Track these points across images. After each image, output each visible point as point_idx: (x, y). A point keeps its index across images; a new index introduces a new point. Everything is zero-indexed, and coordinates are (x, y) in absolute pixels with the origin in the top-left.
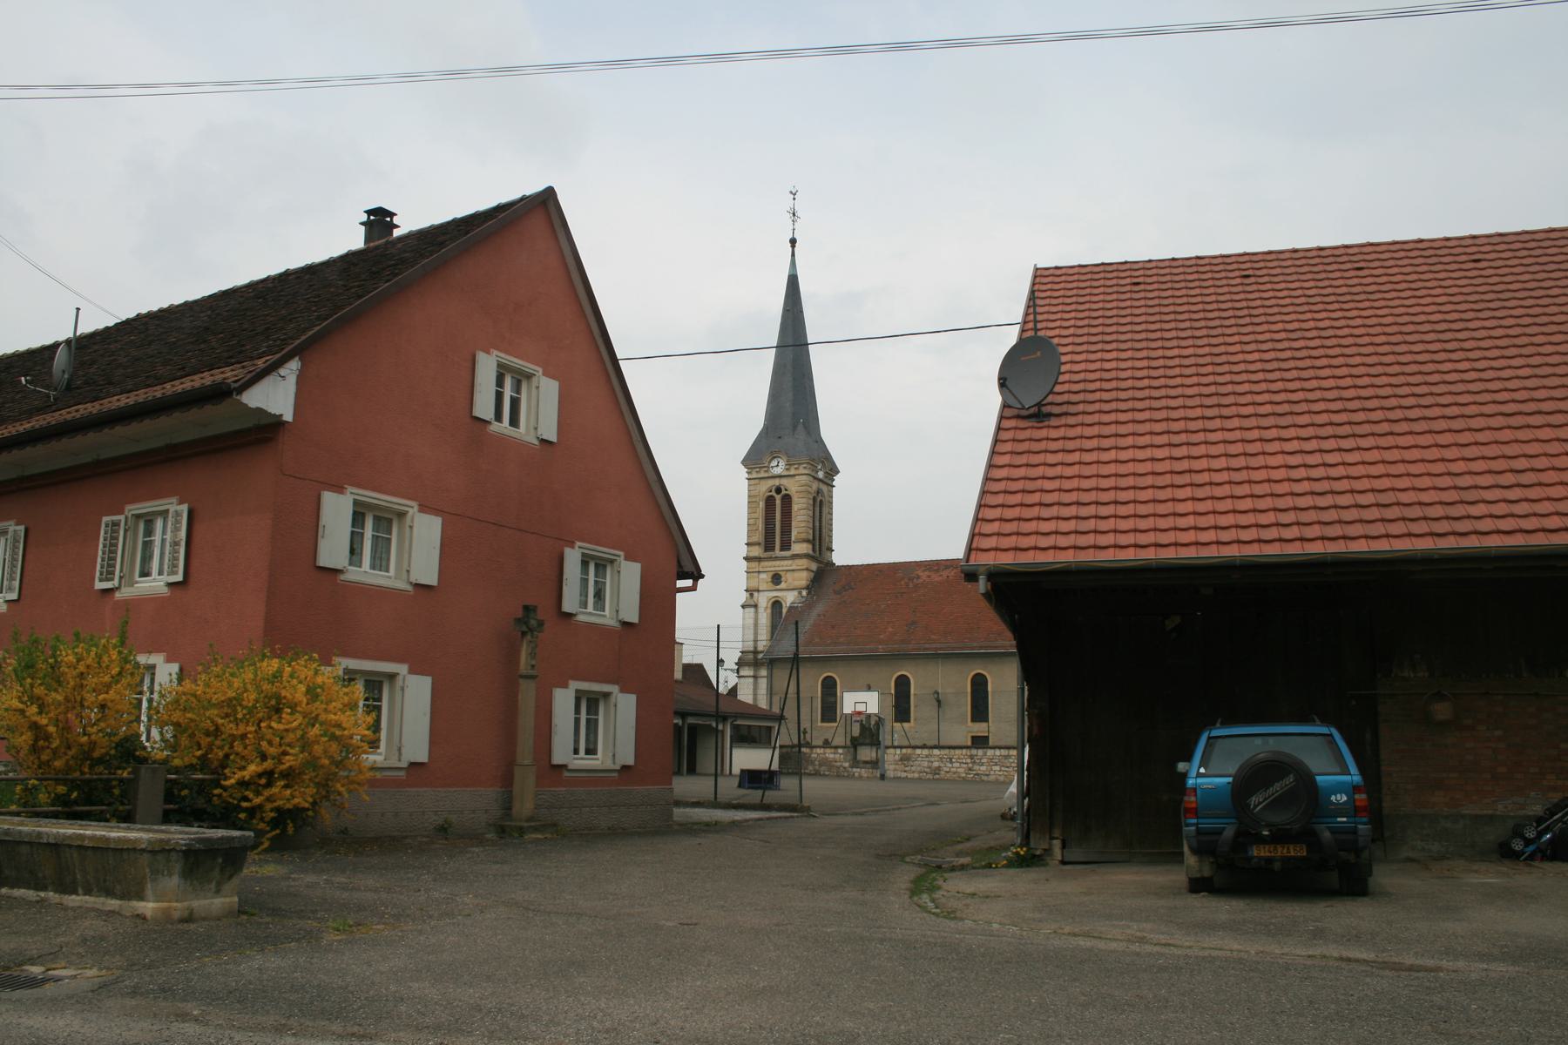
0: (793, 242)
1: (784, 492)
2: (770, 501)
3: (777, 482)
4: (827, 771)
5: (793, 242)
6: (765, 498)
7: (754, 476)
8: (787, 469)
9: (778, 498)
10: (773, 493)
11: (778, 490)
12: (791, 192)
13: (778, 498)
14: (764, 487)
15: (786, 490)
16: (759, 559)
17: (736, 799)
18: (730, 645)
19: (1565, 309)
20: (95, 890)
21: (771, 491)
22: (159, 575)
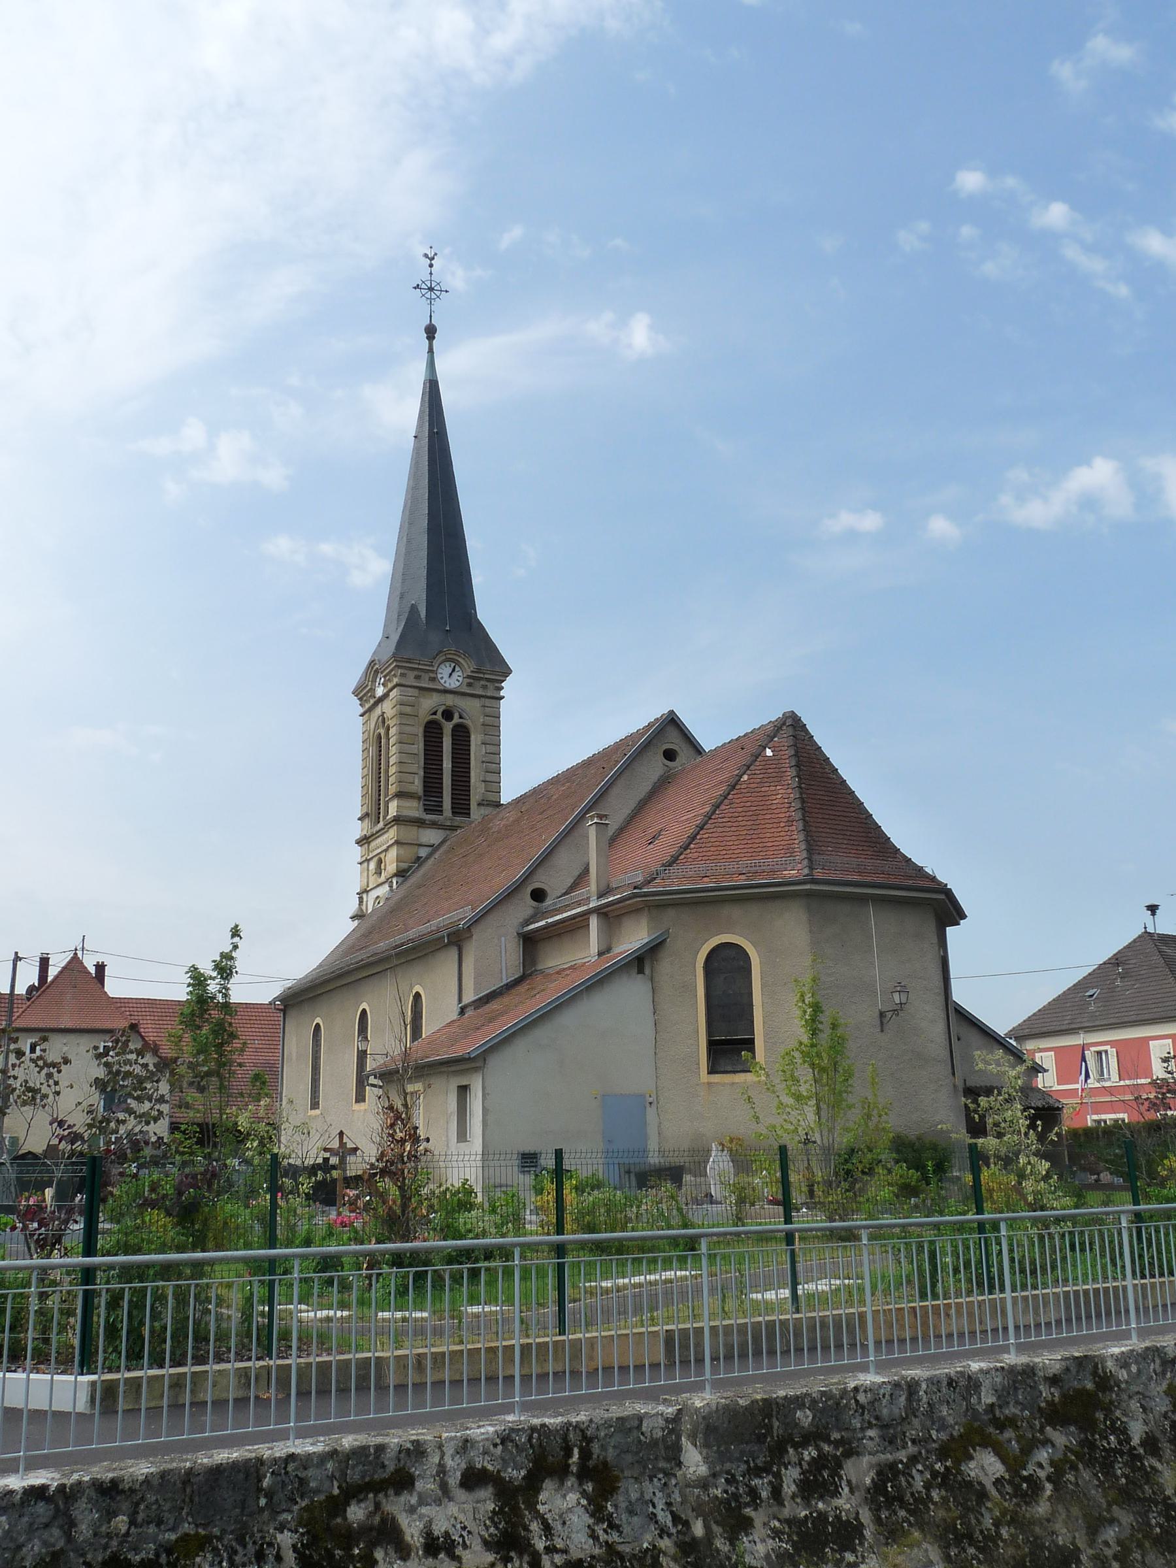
0: (431, 332)
1: (456, 720)
2: (432, 731)
3: (450, 700)
4: (69, 1270)
5: (431, 332)
6: (426, 720)
7: (411, 681)
8: (469, 685)
9: (448, 727)
10: (439, 717)
11: (448, 715)
12: (426, 256)
13: (448, 727)
14: (429, 703)
15: (435, 713)
16: (419, 823)
17: (1098, 1108)
18: (33, 963)
19: (1174, 998)
20: (1012, 1403)
21: (435, 713)
22: (357, 1101)
